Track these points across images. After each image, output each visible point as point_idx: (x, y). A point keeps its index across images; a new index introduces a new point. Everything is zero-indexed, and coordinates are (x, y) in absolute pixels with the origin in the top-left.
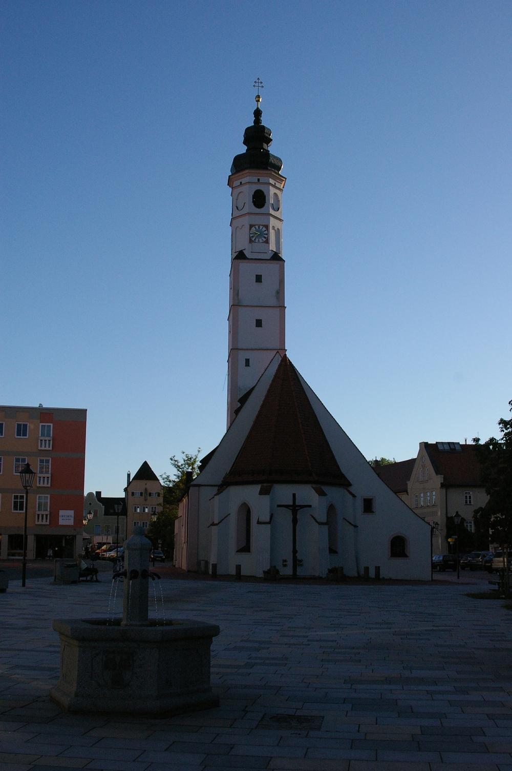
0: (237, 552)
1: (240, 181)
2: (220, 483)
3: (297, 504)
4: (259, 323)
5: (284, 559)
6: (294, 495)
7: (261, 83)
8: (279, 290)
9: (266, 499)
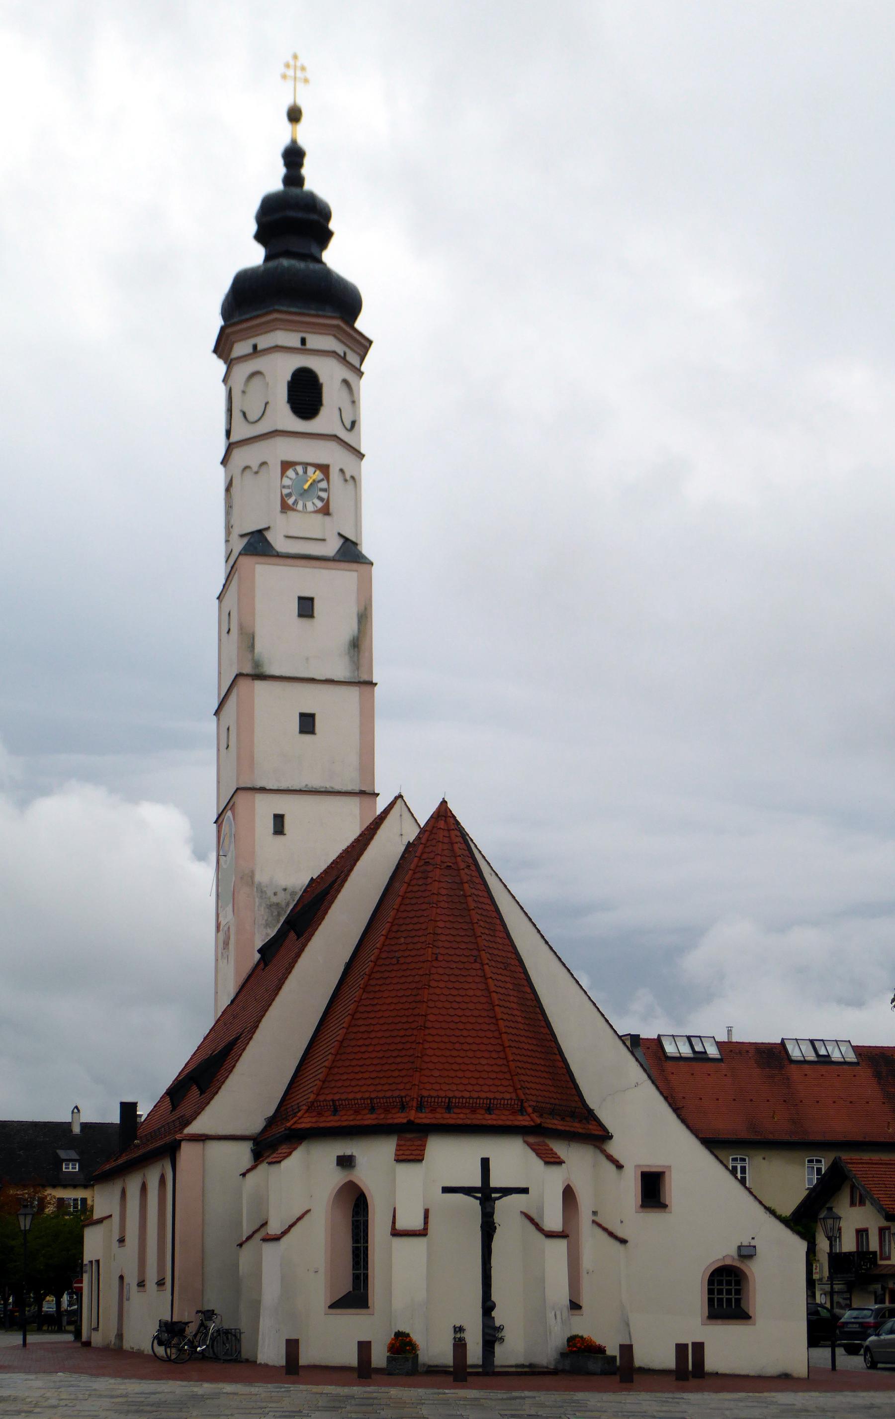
0: (331, 1307)
1: (252, 341)
2: (255, 1124)
4: (307, 723)
5: (458, 1325)
6: (485, 1163)
9: (406, 1171)
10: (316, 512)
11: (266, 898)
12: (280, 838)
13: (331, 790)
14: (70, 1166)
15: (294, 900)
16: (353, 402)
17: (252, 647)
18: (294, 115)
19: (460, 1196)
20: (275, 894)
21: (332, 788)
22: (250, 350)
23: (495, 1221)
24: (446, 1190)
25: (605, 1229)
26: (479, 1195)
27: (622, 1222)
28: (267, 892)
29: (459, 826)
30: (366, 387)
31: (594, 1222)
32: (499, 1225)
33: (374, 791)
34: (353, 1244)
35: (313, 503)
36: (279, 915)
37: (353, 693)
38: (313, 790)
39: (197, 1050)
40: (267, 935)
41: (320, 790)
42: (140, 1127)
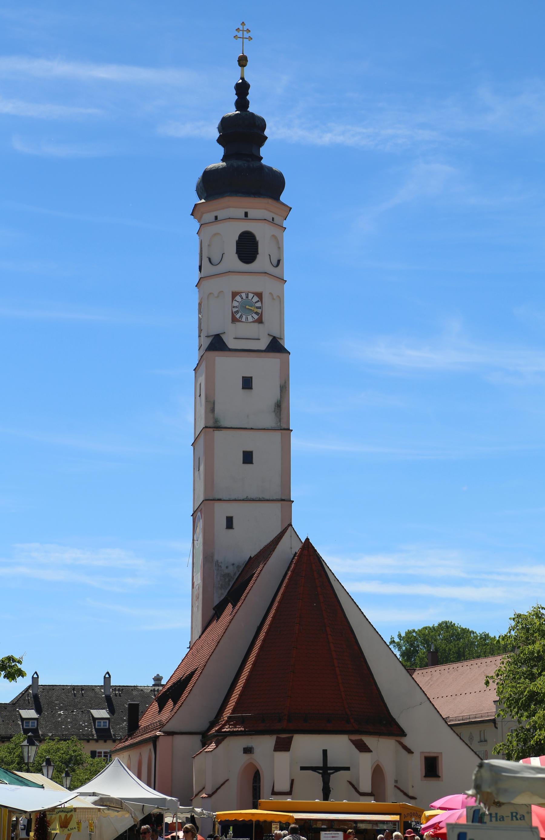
3: (329, 765)
4: (248, 457)
6: (325, 752)
7: (248, 31)
8: (280, 401)
9: (282, 757)
10: (253, 322)
11: (221, 570)
12: (230, 531)
13: (263, 499)
14: (102, 724)
15: (239, 571)
16: (279, 248)
17: (213, 410)
18: (243, 61)
19: (310, 772)
20: (227, 567)
21: (264, 498)
22: (213, 219)
23: (330, 787)
24: (303, 768)
25: (402, 791)
26: (321, 771)
27: (413, 787)
28: (222, 566)
29: (316, 553)
30: (288, 238)
31: (395, 786)
32: (333, 789)
33: (291, 500)
34: (253, 799)
35: (252, 316)
36: (229, 581)
37: (278, 435)
38: (252, 499)
39: (178, 668)
40: (222, 594)
41: (255, 500)
42: (141, 719)
